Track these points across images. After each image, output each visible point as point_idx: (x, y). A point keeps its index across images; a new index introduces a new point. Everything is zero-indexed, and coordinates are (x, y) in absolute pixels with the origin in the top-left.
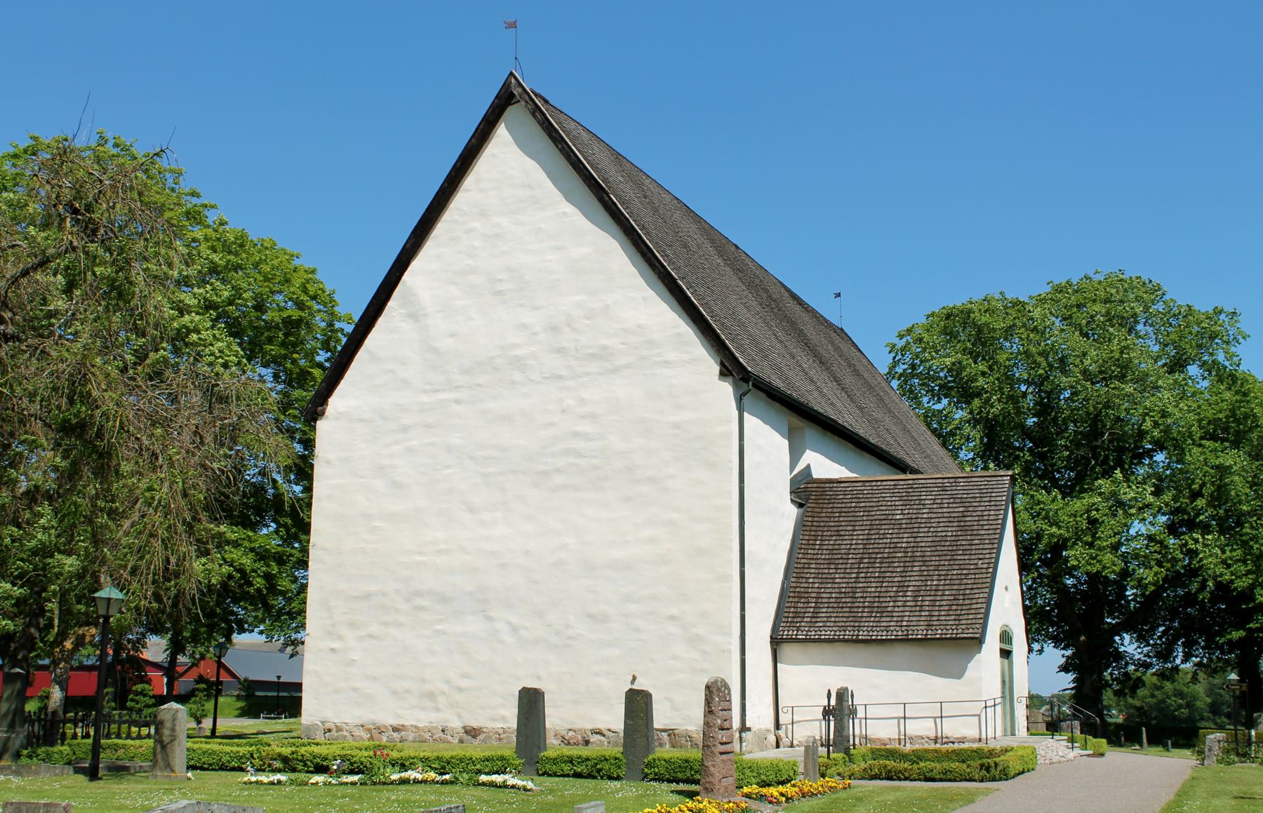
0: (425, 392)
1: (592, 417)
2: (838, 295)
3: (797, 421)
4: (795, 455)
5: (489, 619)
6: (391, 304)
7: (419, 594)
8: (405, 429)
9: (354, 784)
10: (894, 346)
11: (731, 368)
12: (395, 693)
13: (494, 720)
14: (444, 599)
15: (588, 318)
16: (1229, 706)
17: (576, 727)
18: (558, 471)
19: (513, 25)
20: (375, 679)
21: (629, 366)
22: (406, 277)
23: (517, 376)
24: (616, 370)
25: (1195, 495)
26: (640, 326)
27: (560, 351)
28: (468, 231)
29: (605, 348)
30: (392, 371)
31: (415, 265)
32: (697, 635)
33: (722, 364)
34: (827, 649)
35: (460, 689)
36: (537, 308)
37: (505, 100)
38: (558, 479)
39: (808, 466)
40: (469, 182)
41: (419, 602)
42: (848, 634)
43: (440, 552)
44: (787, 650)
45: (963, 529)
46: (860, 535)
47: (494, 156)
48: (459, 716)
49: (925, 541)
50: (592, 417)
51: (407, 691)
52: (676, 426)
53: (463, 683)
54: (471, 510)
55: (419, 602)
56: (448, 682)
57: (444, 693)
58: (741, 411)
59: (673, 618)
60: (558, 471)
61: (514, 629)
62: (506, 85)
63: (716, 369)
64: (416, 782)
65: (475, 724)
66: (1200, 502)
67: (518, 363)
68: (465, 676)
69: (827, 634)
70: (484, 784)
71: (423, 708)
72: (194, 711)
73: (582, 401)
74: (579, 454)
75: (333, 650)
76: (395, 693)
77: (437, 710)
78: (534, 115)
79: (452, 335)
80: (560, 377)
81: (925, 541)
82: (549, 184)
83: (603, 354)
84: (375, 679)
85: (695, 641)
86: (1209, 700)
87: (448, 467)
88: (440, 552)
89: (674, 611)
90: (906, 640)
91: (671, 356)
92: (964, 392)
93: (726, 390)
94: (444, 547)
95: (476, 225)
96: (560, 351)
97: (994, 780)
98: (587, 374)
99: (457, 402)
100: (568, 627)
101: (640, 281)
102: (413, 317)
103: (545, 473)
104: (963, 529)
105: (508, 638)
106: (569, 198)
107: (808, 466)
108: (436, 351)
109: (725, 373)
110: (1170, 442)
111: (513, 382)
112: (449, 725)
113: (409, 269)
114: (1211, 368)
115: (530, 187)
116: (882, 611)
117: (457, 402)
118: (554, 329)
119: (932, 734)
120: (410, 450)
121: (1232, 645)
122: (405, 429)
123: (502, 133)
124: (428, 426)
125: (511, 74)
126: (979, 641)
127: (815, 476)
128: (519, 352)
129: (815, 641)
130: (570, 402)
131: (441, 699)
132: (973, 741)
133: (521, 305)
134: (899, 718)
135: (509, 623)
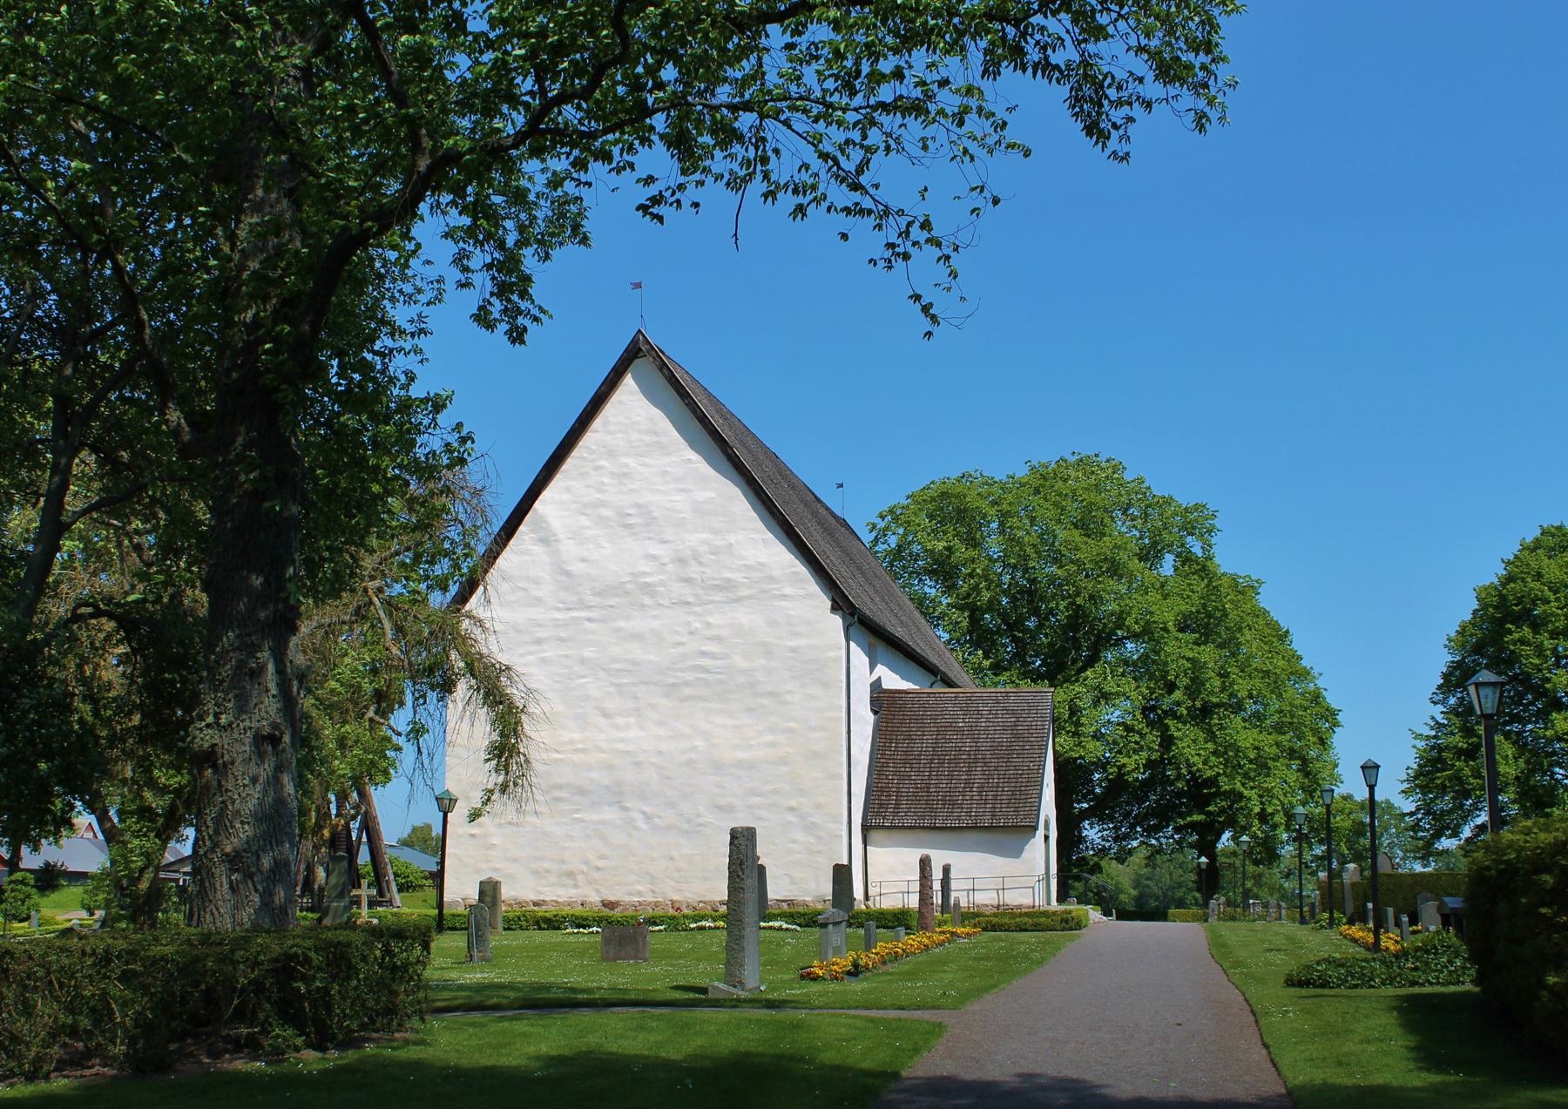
0: (558, 609)
1: (718, 639)
2: (841, 486)
3: (873, 640)
4: (872, 668)
5: (625, 809)
6: (522, 528)
7: (559, 787)
8: (539, 641)
9: (660, 931)
10: (874, 526)
11: (841, 603)
12: (535, 872)
13: (630, 894)
14: (581, 791)
15: (713, 554)
16: (1157, 899)
17: (707, 899)
18: (687, 684)
19: (638, 286)
20: (515, 860)
21: (750, 597)
22: (537, 505)
23: (647, 601)
24: (739, 600)
25: (1171, 687)
26: (760, 564)
27: (688, 580)
28: (597, 468)
29: (729, 580)
30: (525, 590)
31: (546, 495)
32: (813, 823)
33: (833, 600)
34: (909, 835)
35: (598, 869)
36: (665, 542)
37: (635, 352)
38: (687, 691)
39: (879, 678)
40: (597, 423)
41: (557, 794)
42: (927, 823)
43: (576, 751)
44: (875, 835)
45: (1016, 736)
46: (929, 740)
47: (620, 402)
48: (597, 891)
49: (984, 745)
50: (718, 639)
51: (547, 871)
52: (793, 650)
53: (601, 863)
54: (606, 715)
55: (557, 794)
56: (586, 863)
57: (583, 872)
58: (848, 640)
59: (791, 809)
60: (687, 684)
61: (648, 818)
62: (634, 341)
63: (829, 604)
64: (710, 928)
65: (612, 899)
66: (1177, 695)
67: (648, 589)
68: (603, 857)
69: (908, 822)
70: (764, 928)
71: (564, 886)
72: (86, 902)
73: (709, 625)
74: (705, 670)
75: (473, 835)
76: (535, 872)
77: (576, 886)
78: (661, 370)
79: (583, 560)
80: (688, 603)
81: (984, 745)
82: (675, 433)
83: (727, 586)
84: (515, 860)
85: (811, 828)
86: (1134, 893)
87: (582, 677)
88: (576, 751)
89: (793, 803)
90: (975, 828)
91: (788, 591)
92: (943, 570)
93: (837, 621)
94: (580, 746)
95: (603, 463)
96: (688, 580)
97: (1071, 929)
98: (713, 602)
99: (589, 620)
100: (698, 816)
101: (760, 525)
102: (544, 541)
103: (674, 685)
104: (1016, 736)
105: (644, 826)
106: (693, 445)
107: (879, 678)
108: (567, 574)
109: (835, 608)
110: (1146, 633)
111: (643, 606)
112: (588, 899)
113: (540, 498)
114: (1186, 558)
115: (656, 433)
116: (954, 804)
117: (589, 620)
118: (681, 561)
119: (995, 903)
120: (544, 661)
121: (1193, 826)
122: (539, 641)
123: (629, 381)
124: (562, 640)
125: (639, 331)
126: (1035, 828)
127: (884, 686)
128: (648, 580)
129: (899, 828)
130: (698, 625)
131: (580, 877)
132: (1028, 907)
133: (650, 538)
134: (968, 890)
135: (644, 813)
